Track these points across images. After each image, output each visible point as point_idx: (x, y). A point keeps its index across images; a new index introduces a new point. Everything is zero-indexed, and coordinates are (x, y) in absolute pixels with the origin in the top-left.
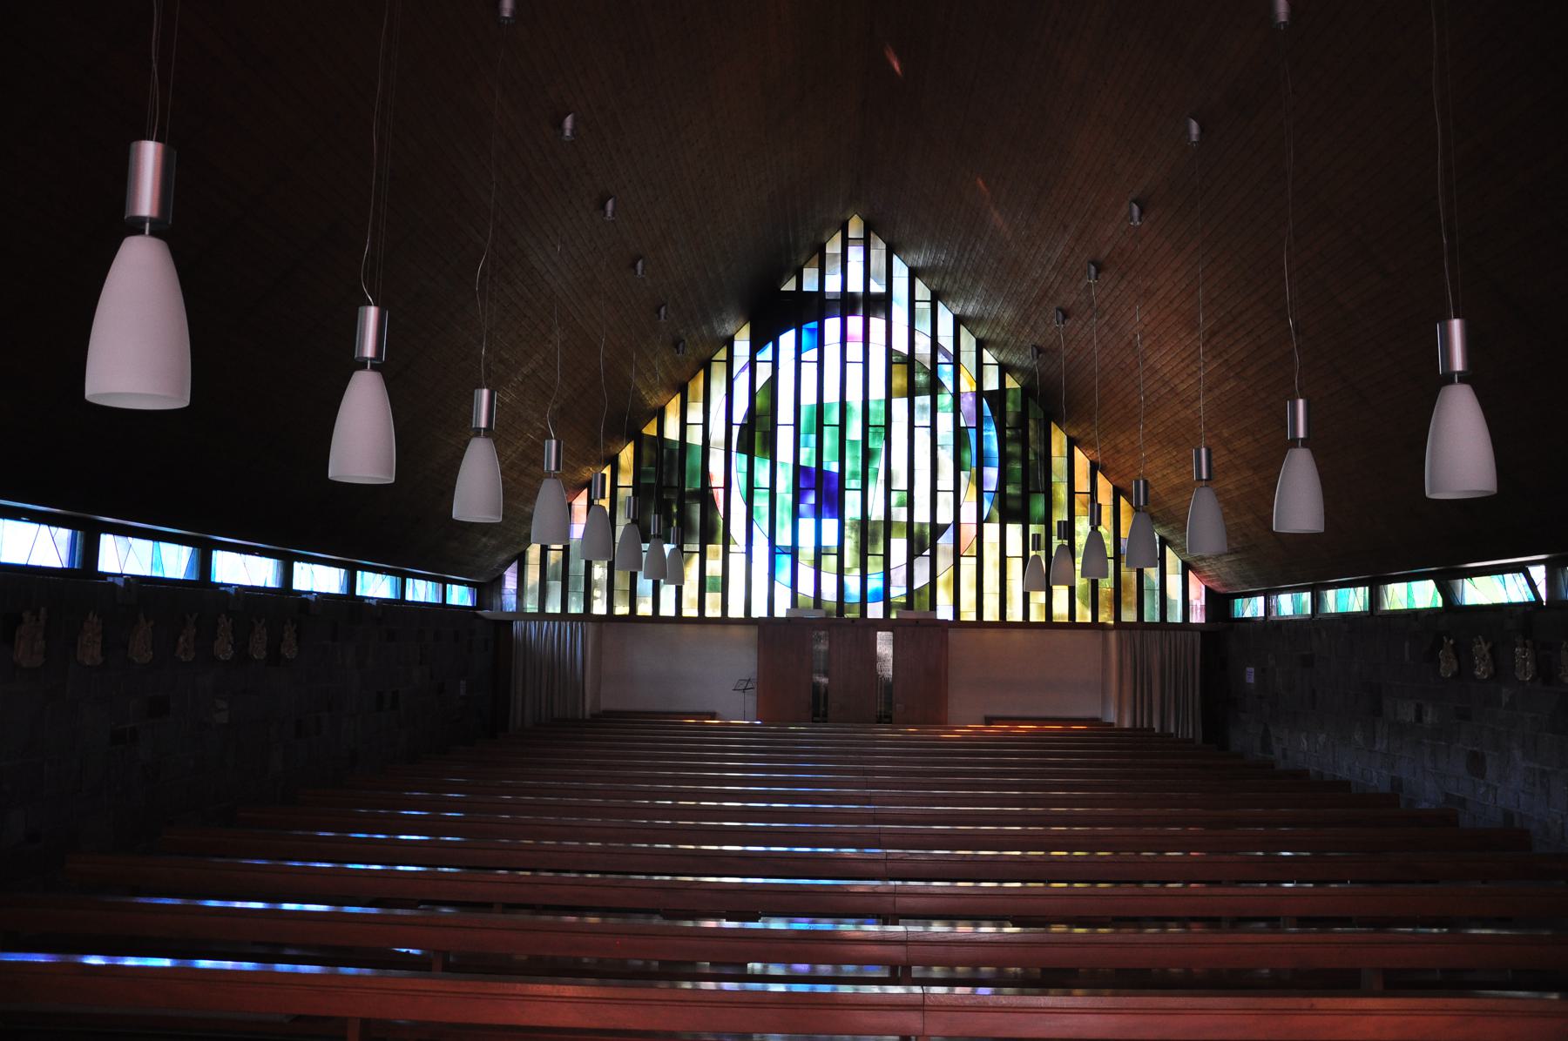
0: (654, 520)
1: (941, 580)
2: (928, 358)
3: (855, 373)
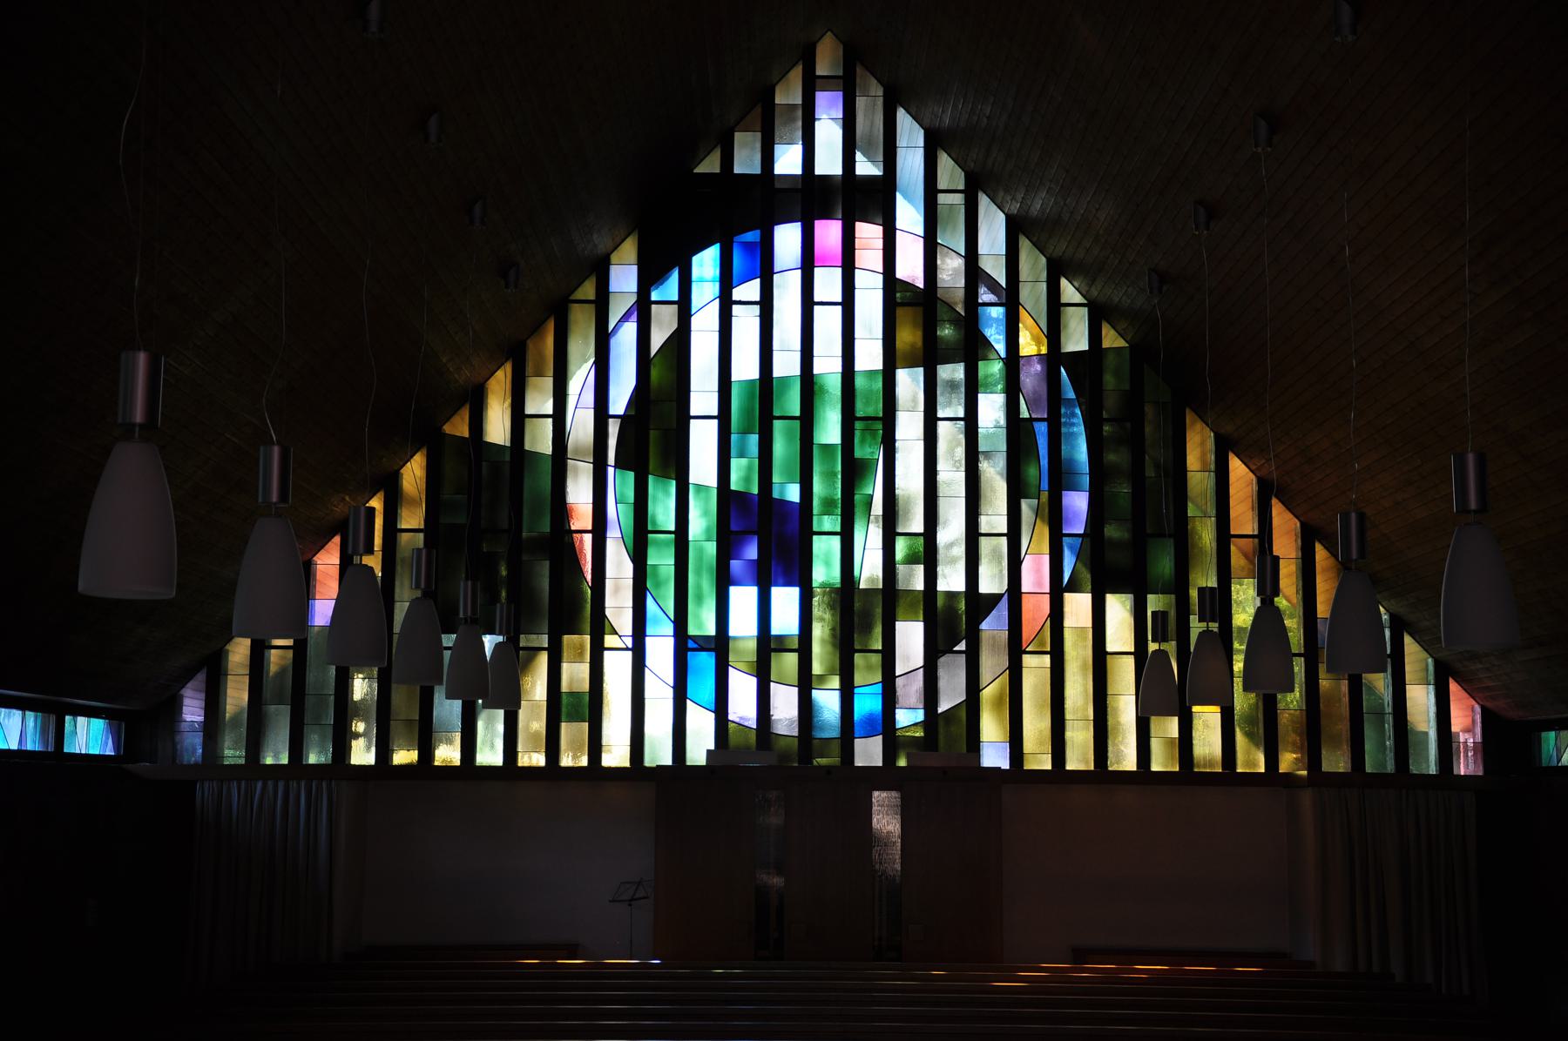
0: (464, 593)
1: (987, 694)
2: (961, 294)
3: (828, 322)
